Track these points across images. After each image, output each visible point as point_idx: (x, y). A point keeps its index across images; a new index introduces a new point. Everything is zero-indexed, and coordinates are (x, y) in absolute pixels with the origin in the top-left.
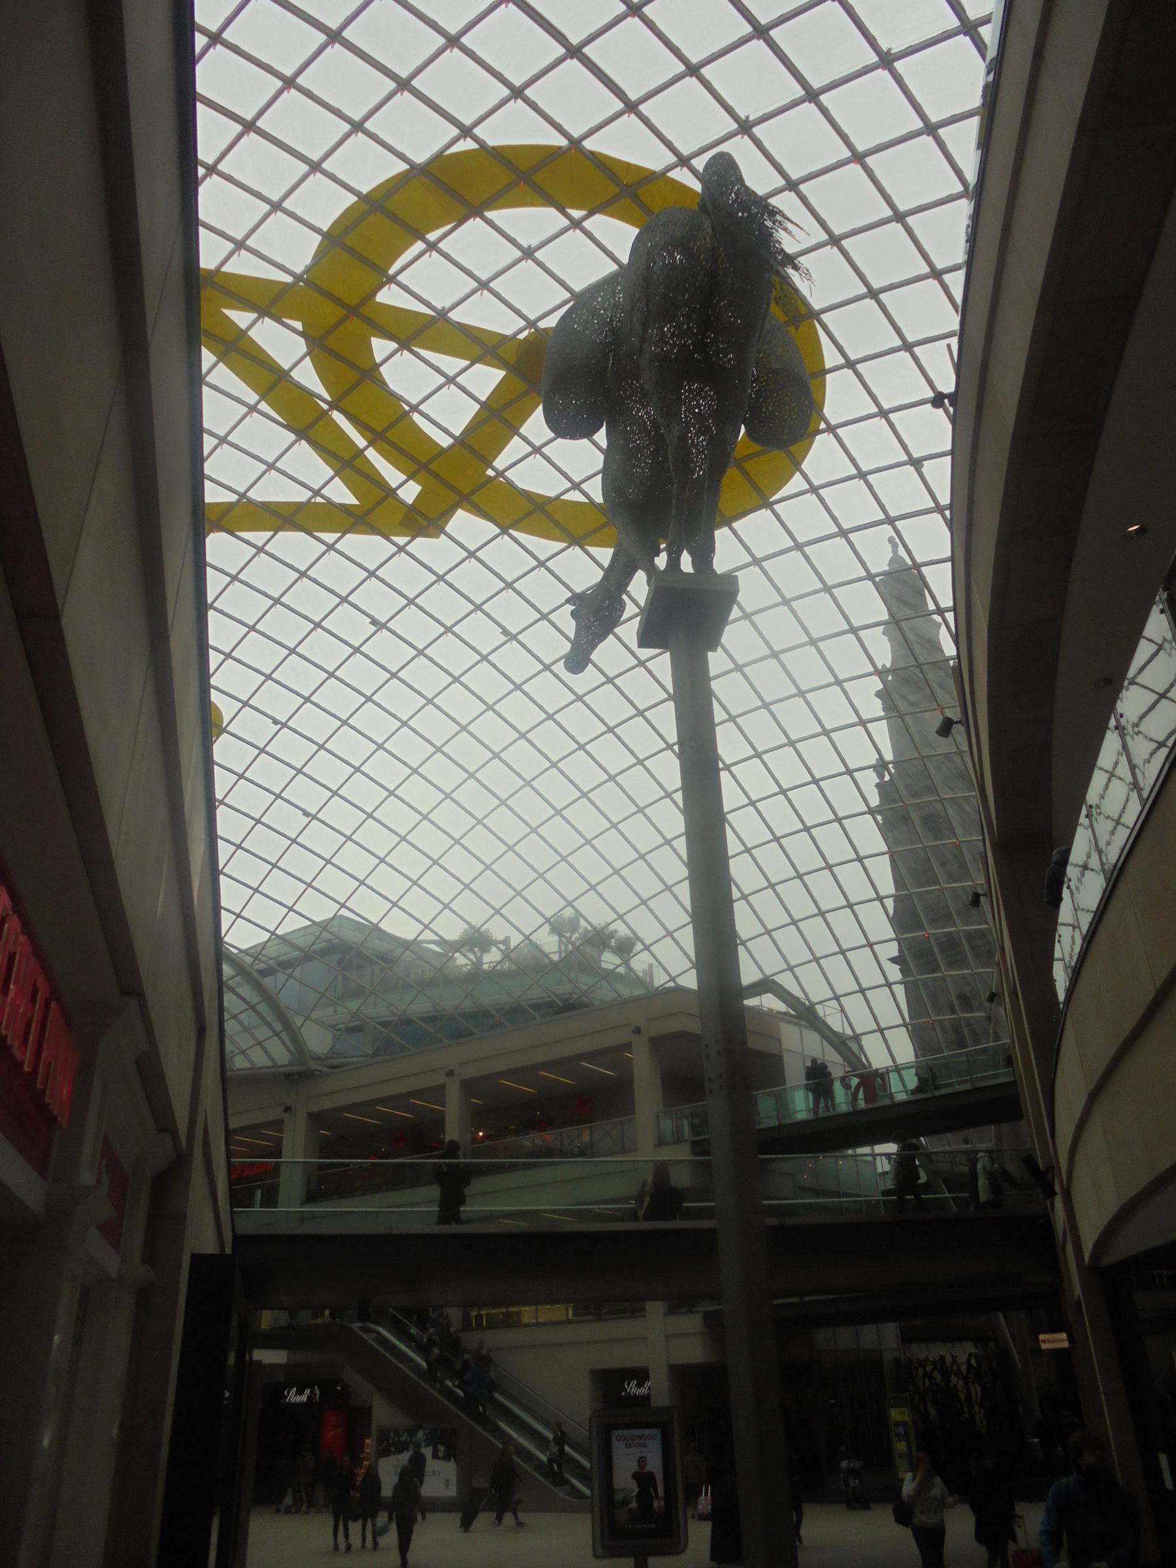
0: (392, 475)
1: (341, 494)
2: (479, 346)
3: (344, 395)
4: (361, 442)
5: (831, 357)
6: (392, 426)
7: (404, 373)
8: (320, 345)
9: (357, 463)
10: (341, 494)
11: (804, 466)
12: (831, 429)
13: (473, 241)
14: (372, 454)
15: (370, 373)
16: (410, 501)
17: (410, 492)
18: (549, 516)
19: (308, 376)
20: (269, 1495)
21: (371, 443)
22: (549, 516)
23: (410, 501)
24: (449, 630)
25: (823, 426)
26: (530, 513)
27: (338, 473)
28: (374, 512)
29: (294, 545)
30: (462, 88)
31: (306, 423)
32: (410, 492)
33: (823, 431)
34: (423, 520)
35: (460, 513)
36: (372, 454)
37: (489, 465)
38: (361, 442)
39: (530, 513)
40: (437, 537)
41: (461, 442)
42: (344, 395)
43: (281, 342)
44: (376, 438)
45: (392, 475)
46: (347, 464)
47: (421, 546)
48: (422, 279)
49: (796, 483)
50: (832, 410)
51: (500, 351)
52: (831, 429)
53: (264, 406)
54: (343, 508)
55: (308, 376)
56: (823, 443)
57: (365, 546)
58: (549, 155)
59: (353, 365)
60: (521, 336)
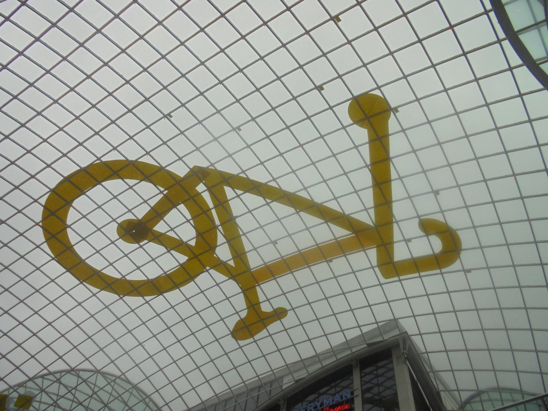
0: (207, 196)
1: (229, 192)
3: (212, 229)
4: (213, 211)
5: (45, 247)
6: (200, 213)
7: (188, 234)
8: (212, 247)
9: (217, 203)
10: (229, 192)
11: (42, 208)
12: (37, 224)
13: (153, 272)
14: (211, 205)
15: (200, 235)
16: (201, 184)
17: (201, 188)
18: (142, 173)
19: (221, 239)
20: (248, 269)
21: (210, 210)
22: (142, 173)
23: (201, 184)
25: (41, 224)
26: (152, 174)
27: (227, 201)
28: (218, 180)
29: (258, 175)
30: (145, 312)
31: (229, 220)
32: (201, 188)
33: (40, 222)
34: (199, 174)
35: (182, 175)
36: (211, 205)
37: (165, 196)
38: (213, 211)
39: (152, 174)
40: (195, 166)
41: (175, 206)
42: (212, 229)
43: (223, 252)
44: (206, 211)
45: (207, 196)
46: (222, 204)
47: (204, 164)
49: (43, 201)
50: (39, 231)
51: (153, 237)
52: (37, 224)
53: (241, 233)
54: (230, 185)
55: (221, 239)
56: (38, 218)
57: (228, 167)
58: (129, 294)
59: (203, 238)
60: (146, 241)
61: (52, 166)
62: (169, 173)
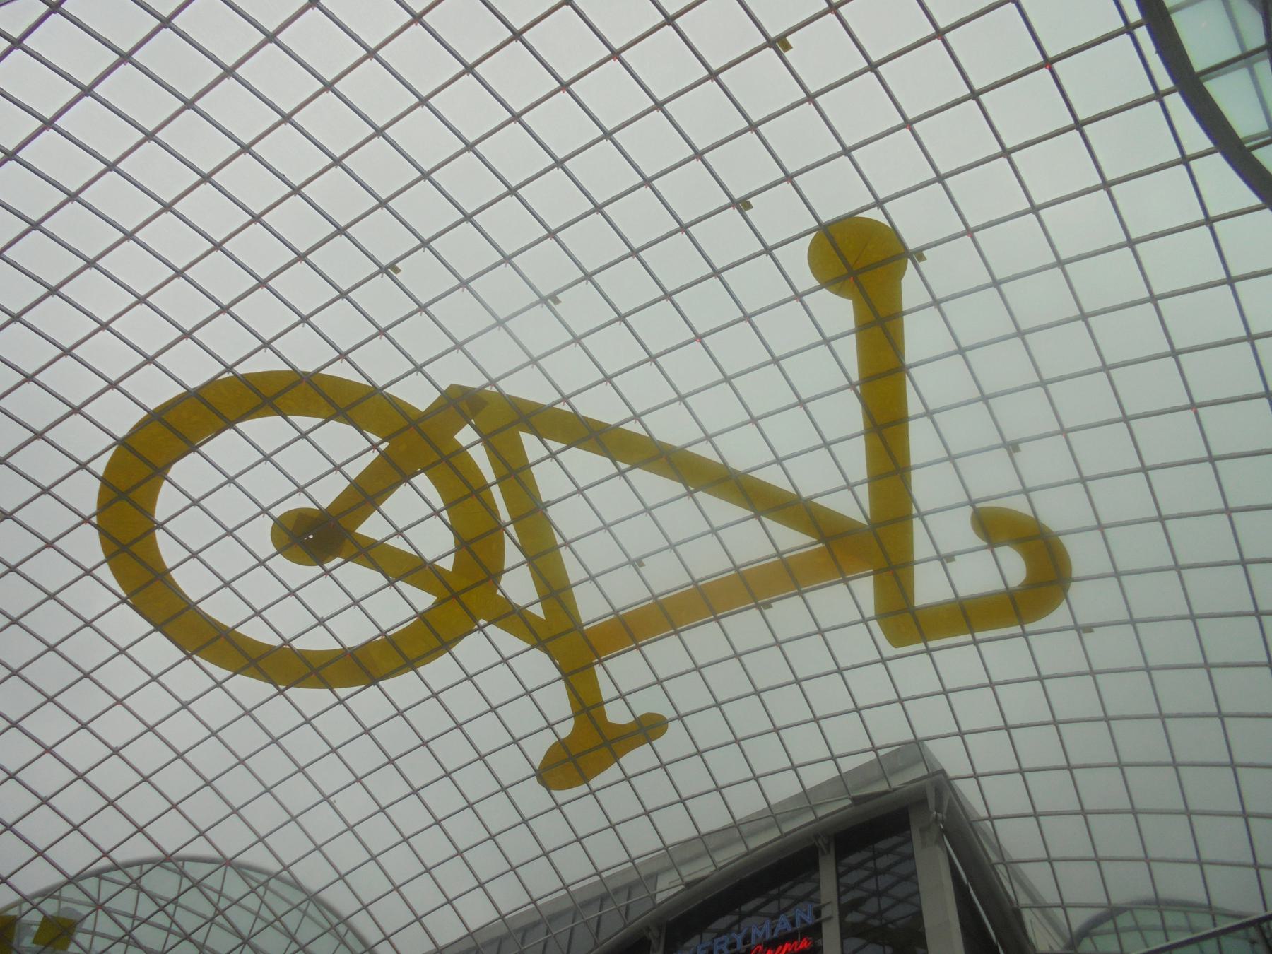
0: (480, 456)
1: (531, 445)
2: (369, 553)
3: (492, 532)
4: (495, 490)
5: (105, 573)
6: (463, 495)
7: (436, 542)
8: (492, 574)
9: (505, 471)
10: (531, 445)
11: (98, 483)
12: (86, 520)
13: (354, 632)
14: (489, 475)
15: (464, 545)
16: (468, 427)
17: (466, 436)
18: (330, 401)
19: (512, 555)
20: (576, 625)
21: (487, 487)
22: (330, 401)
23: (468, 427)
24: (180, 756)
25: (94, 520)
26: (353, 405)
27: (528, 466)
28: (505, 419)
29: (600, 407)
32: (466, 436)
33: (92, 516)
34: (461, 404)
35: (422, 407)
36: (489, 475)
37: (383, 454)
38: (495, 490)
39: (353, 405)
40: (452, 386)
41: (406, 478)
42: (492, 532)
43: (518, 585)
44: (478, 491)
45: (480, 456)
46: (515, 472)
48: (397, 607)
49: (100, 466)
50: (90, 535)
51: (355, 550)
52: (86, 520)
53: (559, 541)
54: (533, 430)
55: (512, 555)
56: (89, 505)
57: (529, 388)
58: (299, 682)
59: (472, 553)
60: (338, 560)
61: (121, 385)
62: (392, 401)
